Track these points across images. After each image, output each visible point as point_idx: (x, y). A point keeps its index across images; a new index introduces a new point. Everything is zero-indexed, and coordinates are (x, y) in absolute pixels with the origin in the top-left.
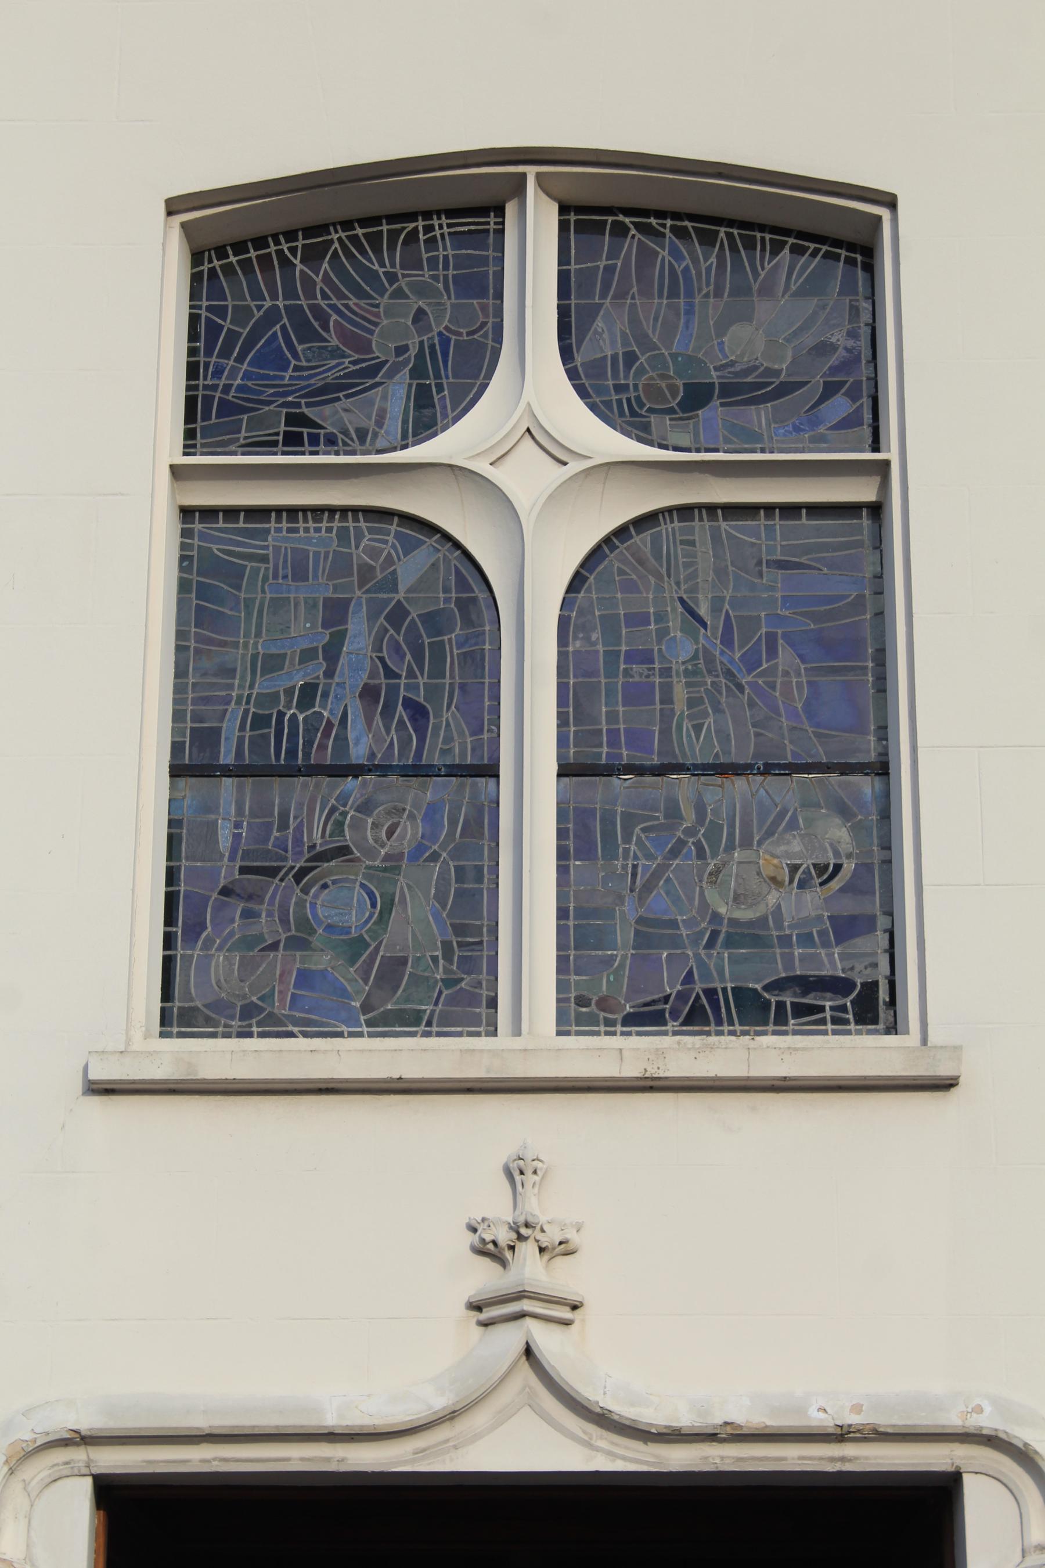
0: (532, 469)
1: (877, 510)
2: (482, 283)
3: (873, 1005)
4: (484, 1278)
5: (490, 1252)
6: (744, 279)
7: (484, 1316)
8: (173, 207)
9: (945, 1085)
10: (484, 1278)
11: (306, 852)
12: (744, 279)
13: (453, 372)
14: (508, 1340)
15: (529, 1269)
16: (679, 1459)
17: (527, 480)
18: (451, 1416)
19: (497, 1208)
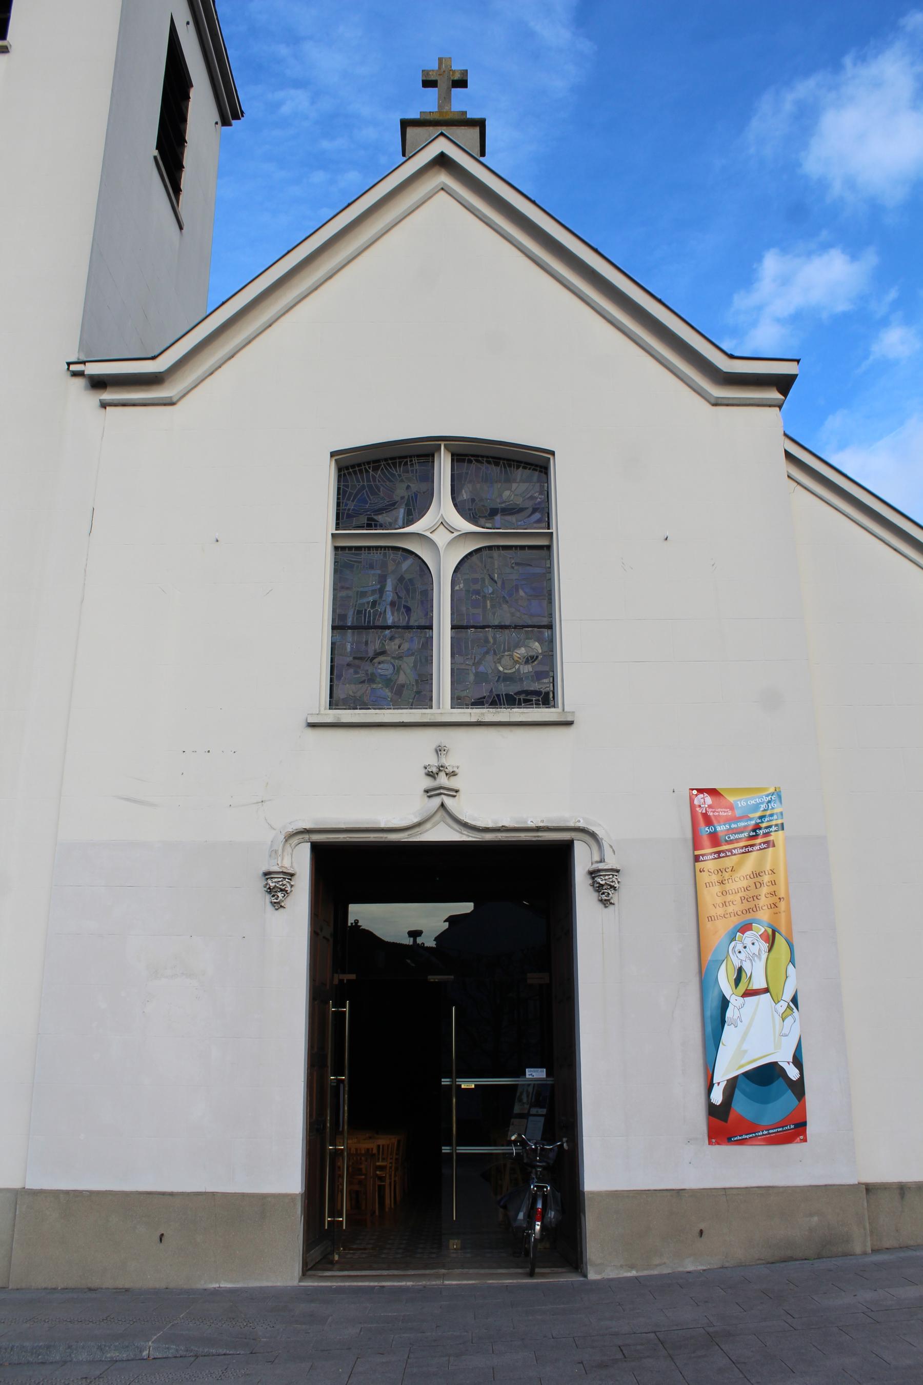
0: (443, 533)
1: (549, 548)
2: (428, 478)
3: (546, 699)
4: (428, 783)
5: (431, 775)
6: (508, 478)
8: (333, 454)
9: (181, 228)
10: (428, 783)
11: (374, 650)
12: (508, 478)
13: (418, 506)
14: (437, 801)
15: (443, 780)
16: (488, 837)
17: (441, 538)
18: (419, 824)
19: (433, 761)
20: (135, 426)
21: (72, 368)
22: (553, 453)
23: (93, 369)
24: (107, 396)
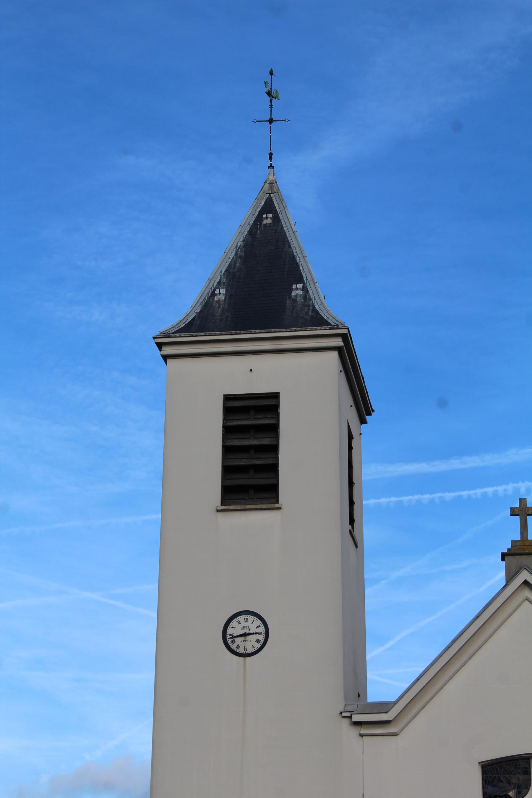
7: (168, 350)
20: (378, 747)
21: (344, 714)
22: (276, 396)
23: (356, 718)
24: (363, 731)
